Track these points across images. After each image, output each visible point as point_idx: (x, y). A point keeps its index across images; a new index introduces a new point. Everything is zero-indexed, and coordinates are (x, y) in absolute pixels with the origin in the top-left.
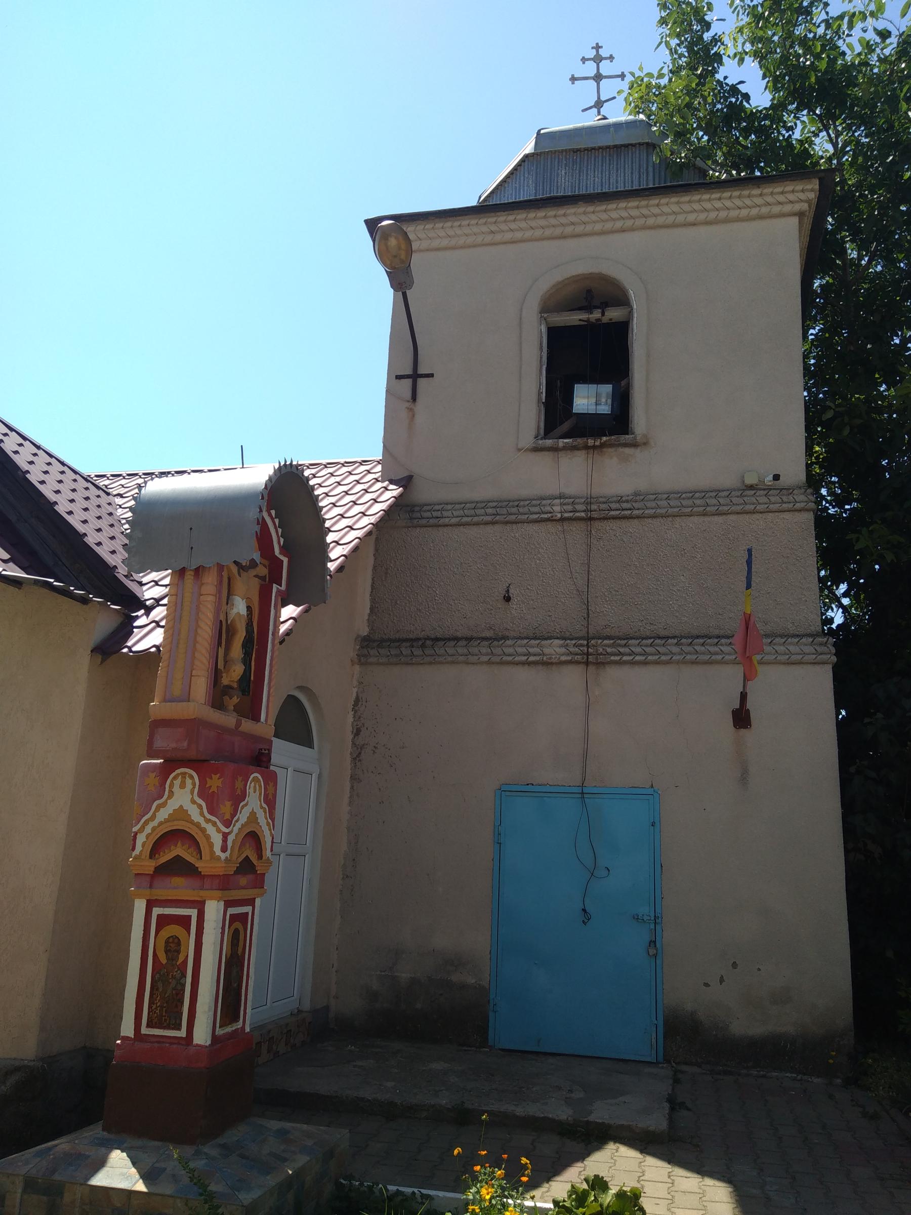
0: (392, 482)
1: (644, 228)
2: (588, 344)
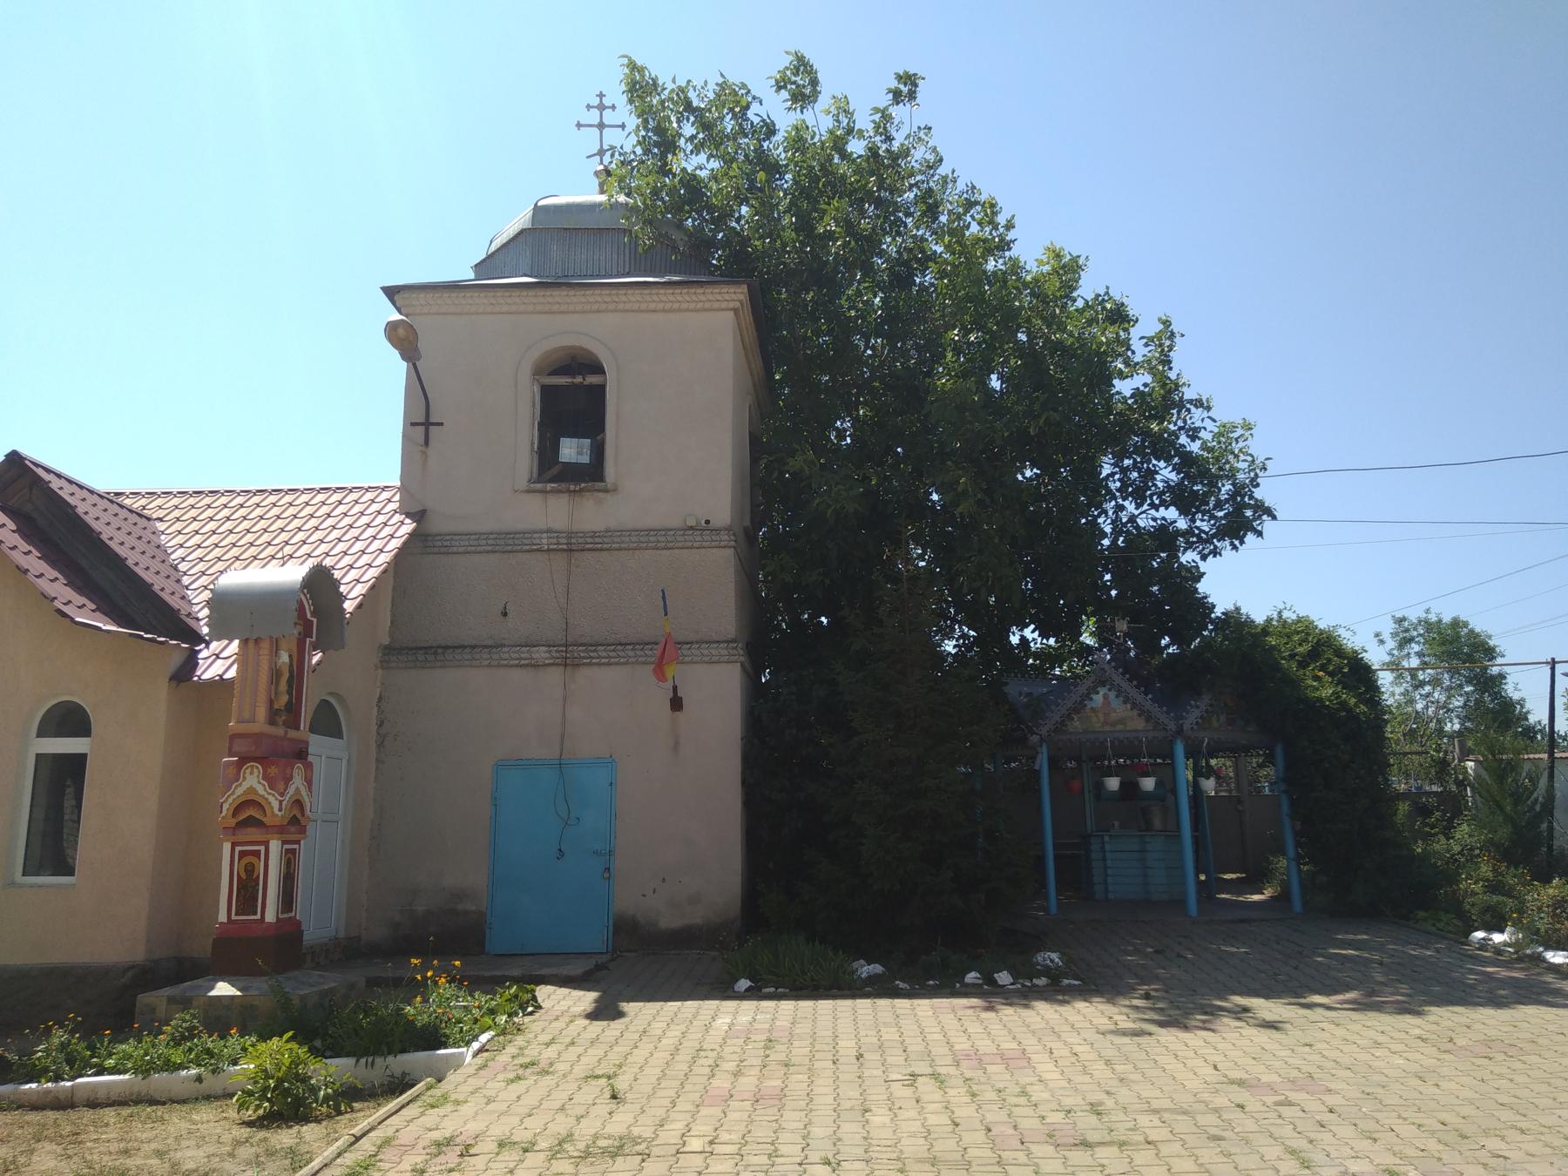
0: (408, 515)
1: (615, 311)
2: (572, 401)
